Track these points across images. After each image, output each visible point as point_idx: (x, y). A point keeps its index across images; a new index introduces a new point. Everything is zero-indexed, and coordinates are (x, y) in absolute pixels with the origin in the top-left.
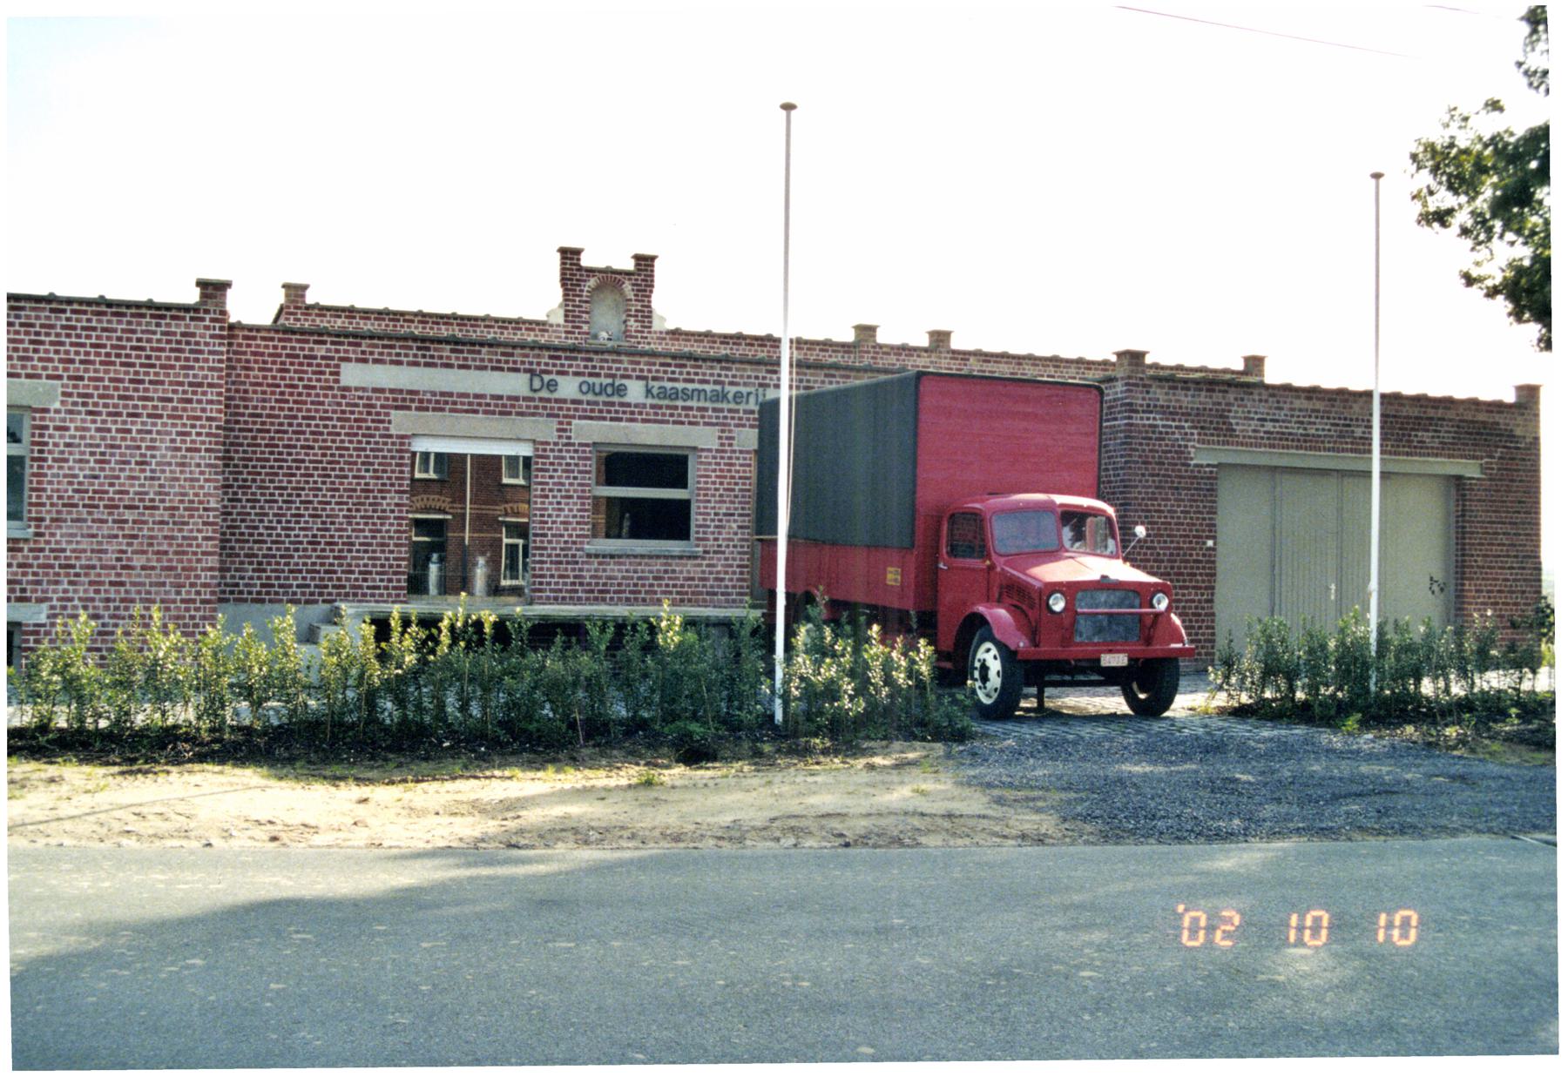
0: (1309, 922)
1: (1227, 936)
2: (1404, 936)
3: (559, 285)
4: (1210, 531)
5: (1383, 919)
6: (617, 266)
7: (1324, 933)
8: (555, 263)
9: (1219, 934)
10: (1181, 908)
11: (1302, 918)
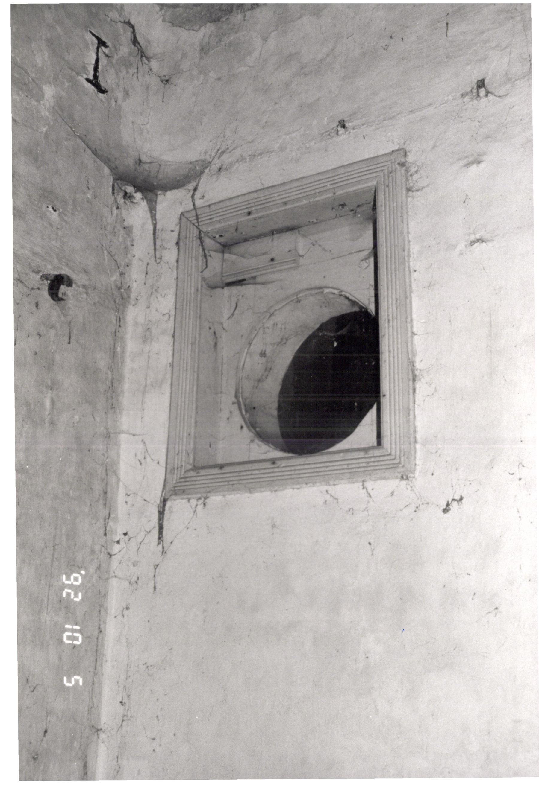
0: (75, 634)
1: (68, 594)
2: (69, 638)
5: (78, 627)
7: (70, 642)
9: (69, 591)
10: (83, 572)
11: (75, 631)
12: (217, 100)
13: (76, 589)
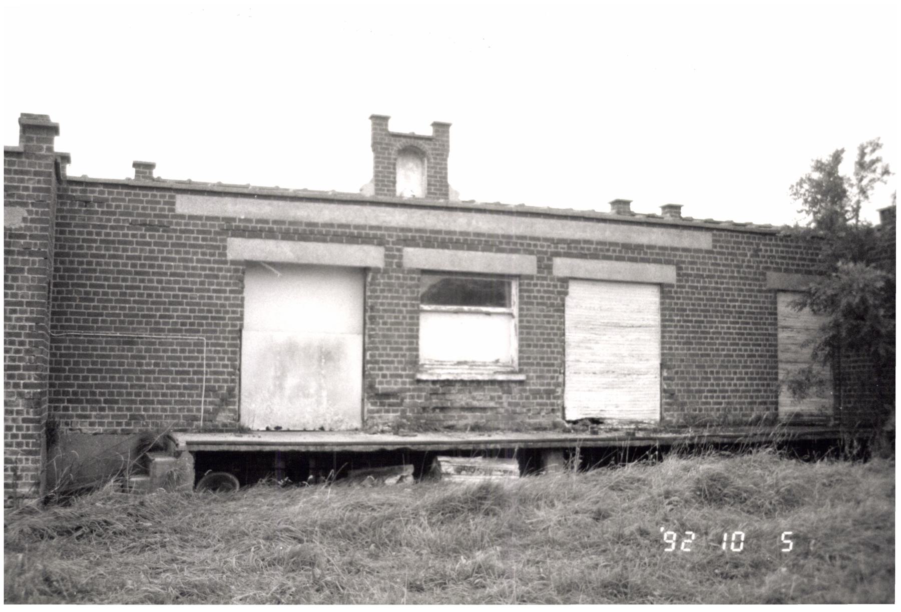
0: (733, 538)
2: (737, 544)
3: (371, 149)
4: (411, 343)
6: (419, 132)
7: (742, 544)
8: (366, 131)
9: (683, 544)
10: (662, 529)
12: (706, 534)
13: (681, 536)
